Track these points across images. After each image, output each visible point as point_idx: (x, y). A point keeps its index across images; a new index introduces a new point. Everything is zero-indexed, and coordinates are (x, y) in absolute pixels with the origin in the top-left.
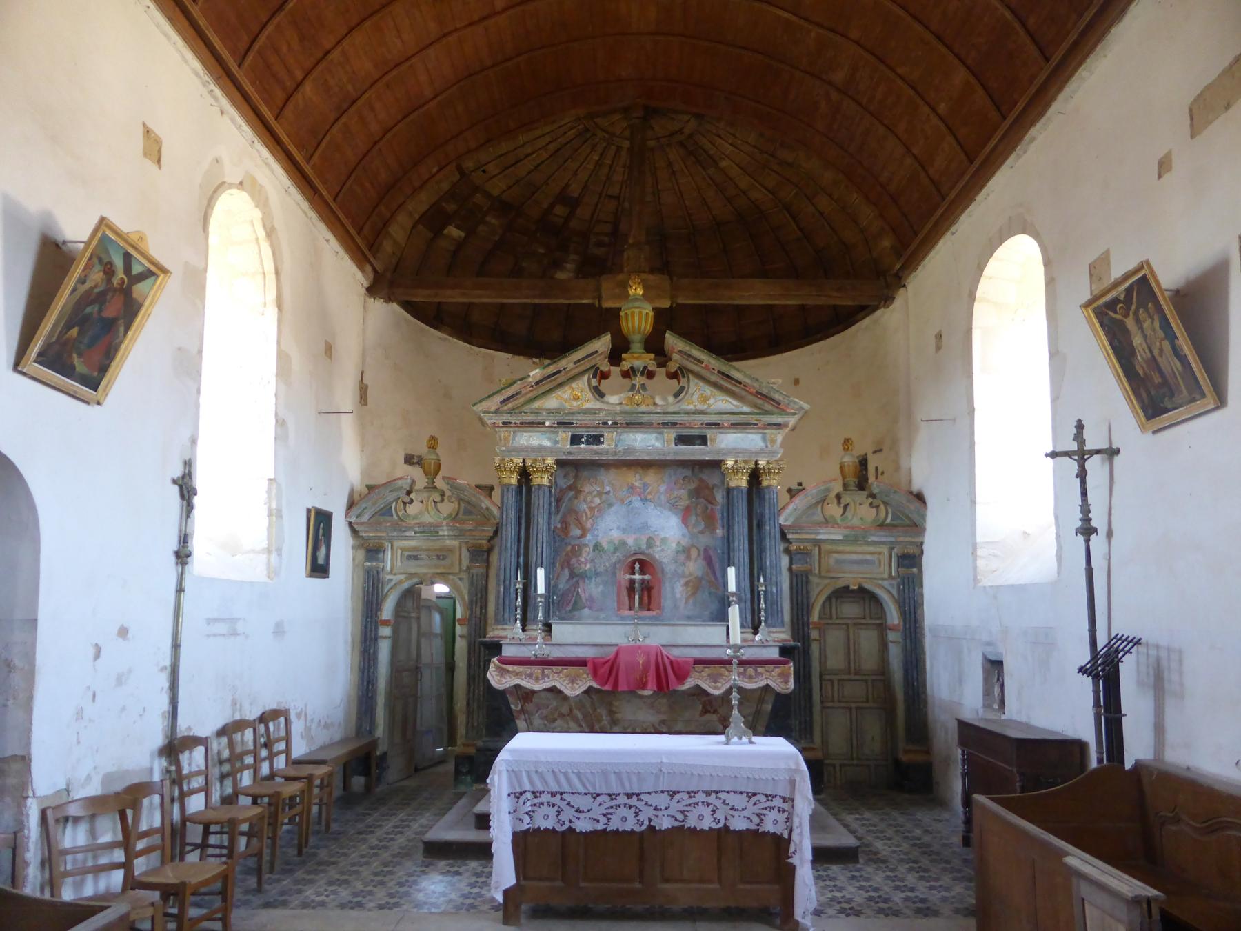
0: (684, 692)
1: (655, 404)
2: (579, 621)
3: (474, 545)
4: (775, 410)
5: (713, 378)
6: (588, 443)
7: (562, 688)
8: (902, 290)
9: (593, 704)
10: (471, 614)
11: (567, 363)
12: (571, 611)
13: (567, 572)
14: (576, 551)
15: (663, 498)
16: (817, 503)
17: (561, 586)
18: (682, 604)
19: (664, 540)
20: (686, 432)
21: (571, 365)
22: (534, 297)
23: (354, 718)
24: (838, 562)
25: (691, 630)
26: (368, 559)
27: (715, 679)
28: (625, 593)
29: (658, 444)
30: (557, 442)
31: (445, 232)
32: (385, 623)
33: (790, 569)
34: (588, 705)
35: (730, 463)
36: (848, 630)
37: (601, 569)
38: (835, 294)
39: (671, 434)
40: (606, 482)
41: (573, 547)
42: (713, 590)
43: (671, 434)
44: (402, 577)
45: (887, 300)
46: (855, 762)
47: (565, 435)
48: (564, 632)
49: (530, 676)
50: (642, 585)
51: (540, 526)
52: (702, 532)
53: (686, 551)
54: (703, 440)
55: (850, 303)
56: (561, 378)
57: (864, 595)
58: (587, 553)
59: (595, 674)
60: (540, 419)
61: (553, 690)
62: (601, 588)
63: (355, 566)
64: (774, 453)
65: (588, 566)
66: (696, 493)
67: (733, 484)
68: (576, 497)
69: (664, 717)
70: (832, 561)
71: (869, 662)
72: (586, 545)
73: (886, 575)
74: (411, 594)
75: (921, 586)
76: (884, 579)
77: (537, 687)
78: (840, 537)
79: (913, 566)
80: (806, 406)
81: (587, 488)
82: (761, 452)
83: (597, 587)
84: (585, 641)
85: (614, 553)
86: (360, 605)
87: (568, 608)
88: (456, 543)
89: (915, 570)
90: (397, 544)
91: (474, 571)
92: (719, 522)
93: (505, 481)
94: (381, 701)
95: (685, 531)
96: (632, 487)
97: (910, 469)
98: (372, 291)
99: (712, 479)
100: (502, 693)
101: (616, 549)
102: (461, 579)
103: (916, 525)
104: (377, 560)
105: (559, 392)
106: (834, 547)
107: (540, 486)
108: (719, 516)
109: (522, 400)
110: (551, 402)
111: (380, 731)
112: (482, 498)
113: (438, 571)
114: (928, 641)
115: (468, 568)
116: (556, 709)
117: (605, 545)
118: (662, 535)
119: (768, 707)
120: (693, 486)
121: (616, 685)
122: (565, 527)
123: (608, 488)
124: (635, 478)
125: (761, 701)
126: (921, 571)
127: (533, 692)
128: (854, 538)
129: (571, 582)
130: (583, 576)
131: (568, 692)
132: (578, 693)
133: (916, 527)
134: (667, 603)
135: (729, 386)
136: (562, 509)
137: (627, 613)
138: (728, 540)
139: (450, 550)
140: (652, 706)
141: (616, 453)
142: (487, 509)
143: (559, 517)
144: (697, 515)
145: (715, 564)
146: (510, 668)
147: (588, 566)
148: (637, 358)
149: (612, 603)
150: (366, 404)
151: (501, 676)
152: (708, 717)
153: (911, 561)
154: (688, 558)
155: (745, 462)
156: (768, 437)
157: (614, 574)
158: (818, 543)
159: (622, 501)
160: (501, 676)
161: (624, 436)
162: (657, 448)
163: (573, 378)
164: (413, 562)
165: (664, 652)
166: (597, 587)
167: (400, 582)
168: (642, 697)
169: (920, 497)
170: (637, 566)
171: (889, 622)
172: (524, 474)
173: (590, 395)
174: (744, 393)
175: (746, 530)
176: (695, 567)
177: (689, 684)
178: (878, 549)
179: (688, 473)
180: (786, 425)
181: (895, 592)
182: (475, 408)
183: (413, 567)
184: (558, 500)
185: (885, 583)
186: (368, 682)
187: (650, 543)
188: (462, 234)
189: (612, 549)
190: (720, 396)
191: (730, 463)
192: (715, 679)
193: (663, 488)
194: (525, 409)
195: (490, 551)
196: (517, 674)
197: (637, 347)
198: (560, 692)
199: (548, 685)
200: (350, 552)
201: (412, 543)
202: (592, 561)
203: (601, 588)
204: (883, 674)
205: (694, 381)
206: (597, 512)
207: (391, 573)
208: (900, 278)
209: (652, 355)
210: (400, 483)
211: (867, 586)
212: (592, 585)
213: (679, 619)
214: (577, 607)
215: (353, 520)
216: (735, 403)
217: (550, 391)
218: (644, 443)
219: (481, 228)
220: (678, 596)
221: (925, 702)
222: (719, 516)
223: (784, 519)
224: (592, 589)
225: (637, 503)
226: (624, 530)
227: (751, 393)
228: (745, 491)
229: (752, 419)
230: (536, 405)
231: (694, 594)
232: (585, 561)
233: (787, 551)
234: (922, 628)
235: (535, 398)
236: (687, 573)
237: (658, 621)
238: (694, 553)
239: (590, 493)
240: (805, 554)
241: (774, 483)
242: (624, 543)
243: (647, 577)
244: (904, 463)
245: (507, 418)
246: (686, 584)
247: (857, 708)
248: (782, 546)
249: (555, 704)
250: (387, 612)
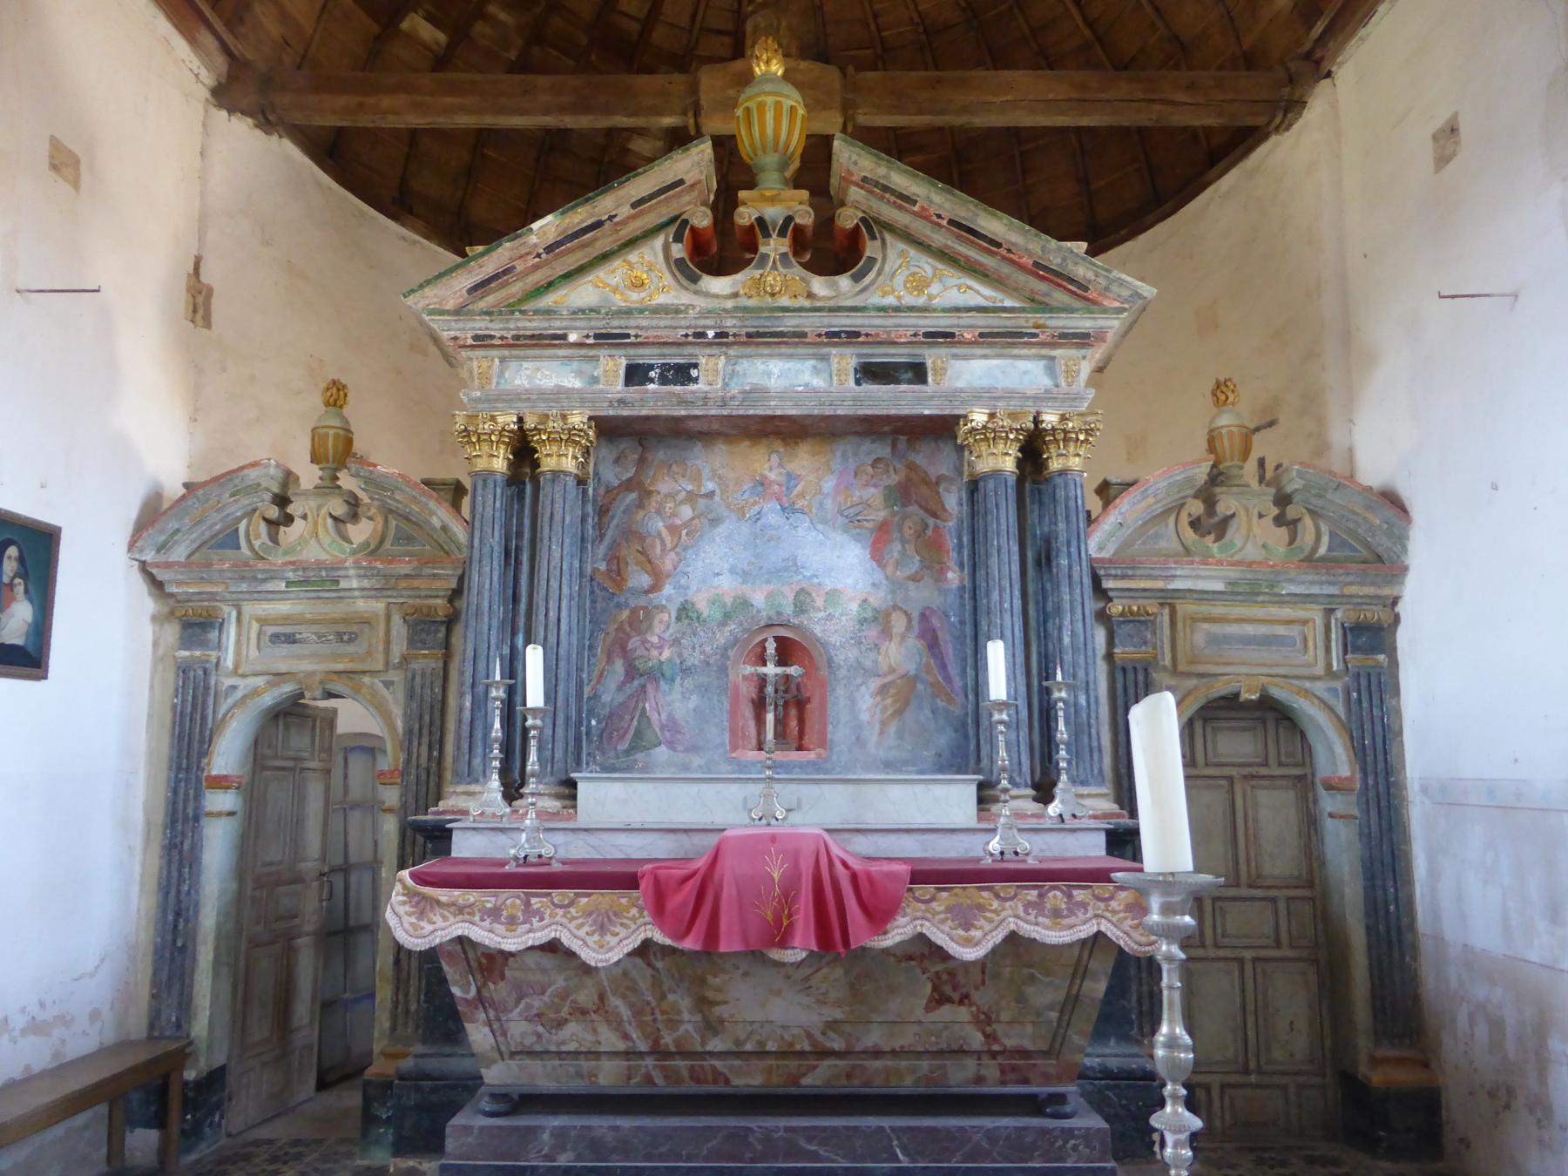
0: (886, 952)
1: (810, 295)
2: (646, 773)
3: (418, 610)
4: (1077, 304)
5: (940, 239)
6: (664, 380)
7: (575, 946)
8: (1324, 84)
9: (656, 983)
10: (408, 762)
11: (614, 202)
12: (627, 752)
13: (619, 666)
14: (640, 621)
15: (829, 504)
16: (1166, 513)
17: (606, 698)
18: (872, 736)
19: (833, 596)
20: (881, 355)
21: (625, 211)
22: (562, 109)
23: (145, 992)
24: (1214, 640)
25: (895, 791)
26: (186, 643)
27: (964, 918)
28: (748, 712)
29: (818, 382)
30: (595, 380)
31: (405, 25)
32: (221, 783)
33: (1109, 656)
34: (644, 985)
35: (979, 417)
36: (1232, 785)
37: (694, 659)
38: (1181, 97)
39: (846, 360)
40: (706, 473)
41: (634, 611)
42: (940, 703)
43: (846, 360)
44: (260, 681)
45: (1289, 107)
46: (1253, 1078)
47: (613, 364)
48: (602, 797)
49: (495, 913)
50: (786, 699)
51: (556, 561)
52: (915, 578)
53: (881, 619)
54: (918, 373)
55: (1211, 121)
56: (604, 241)
57: (1271, 714)
58: (663, 626)
59: (659, 908)
60: (556, 326)
61: (553, 947)
62: (694, 701)
63: (158, 660)
64: (1076, 398)
65: (666, 654)
66: (902, 494)
67: (984, 465)
68: (640, 505)
69: (838, 1014)
70: (1199, 639)
71: (1279, 860)
72: (662, 608)
73: (1319, 670)
74: (289, 713)
75: (1396, 691)
76: (1318, 678)
77: (511, 944)
78: (1219, 586)
79: (1374, 649)
80: (1148, 291)
81: (664, 486)
82: (1047, 397)
83: (685, 697)
84: (636, 820)
85: (723, 624)
86: (165, 745)
87: (623, 746)
88: (379, 606)
89: (1381, 657)
90: (250, 609)
91: (416, 666)
92: (954, 555)
93: (481, 464)
94: (205, 955)
95: (878, 576)
96: (763, 483)
97: (1351, 450)
98: (224, 95)
99: (935, 461)
100: (431, 956)
101: (727, 616)
102: (388, 684)
103: (1380, 559)
104: (204, 644)
105: (601, 273)
106: (1204, 609)
107: (557, 474)
108: (951, 542)
109: (517, 288)
110: (583, 293)
111: (200, 1027)
112: (432, 505)
113: (340, 667)
114: (1418, 814)
115: (405, 659)
116: (564, 995)
117: (703, 606)
118: (829, 584)
119: (1098, 987)
120: (894, 479)
121: (712, 935)
122: (617, 570)
123: (710, 486)
124: (767, 463)
125: (1080, 971)
126: (1394, 663)
127: (506, 955)
128: (1246, 592)
129: (629, 689)
130: (655, 675)
131: (588, 956)
132: (615, 956)
133: (1385, 564)
134: (839, 733)
135: (973, 254)
136: (610, 534)
137: (753, 755)
138: (974, 593)
139: (366, 622)
140: (806, 986)
141: (724, 403)
142: (445, 528)
143: (602, 549)
144: (903, 541)
145: (951, 647)
146: (443, 894)
147: (666, 654)
148: (772, 200)
149: (718, 735)
150: (208, 324)
151: (421, 915)
152: (945, 1012)
153: (1372, 636)
154: (886, 633)
155: (1013, 416)
156: (1060, 367)
157: (723, 670)
158: (1168, 599)
159: (741, 512)
160: (421, 915)
161: (744, 365)
162: (815, 391)
163: (631, 243)
164: (284, 649)
165: (836, 850)
166: (685, 697)
167: (256, 692)
168: (779, 965)
169: (1392, 501)
170: (771, 647)
171: (1323, 769)
172: (523, 450)
173: (668, 279)
174: (1006, 269)
175: (1016, 568)
176: (902, 654)
177: (899, 932)
178: (1300, 613)
179: (883, 450)
180: (1100, 336)
181: (1341, 710)
182: (410, 301)
183: (282, 659)
184: (603, 512)
185: (1319, 687)
186: (178, 914)
187: (802, 602)
188: (442, 37)
189: (718, 615)
190: (953, 278)
191: (979, 417)
192: (964, 918)
193: (828, 485)
194: (529, 306)
195: (451, 621)
196: (460, 910)
197: (771, 181)
198: (571, 955)
199: (540, 937)
200: (147, 631)
201: (284, 608)
202: (676, 642)
203: (694, 701)
204: (1310, 885)
205: (895, 246)
206: (686, 536)
207: (235, 672)
208: (1318, 63)
209: (805, 194)
210: (253, 474)
211: (1276, 693)
212: (676, 695)
213: (867, 768)
214: (640, 743)
215: (149, 556)
216: (987, 291)
217: (581, 270)
218: (789, 380)
219: (480, 28)
220: (865, 717)
221: (1415, 948)
222: (951, 542)
223: (1100, 542)
224: (675, 703)
225: (772, 514)
226: (745, 576)
227: (1022, 268)
228: (1012, 480)
229: (1025, 321)
230: (548, 300)
231: (899, 713)
232: (661, 641)
233: (1102, 617)
234: (1400, 786)
235: (550, 286)
236: (884, 667)
237: (820, 773)
238: (898, 623)
239: (671, 496)
240: (1140, 621)
241: (1075, 463)
242: (744, 604)
243: (794, 670)
244: (1336, 436)
245: (481, 325)
246: (883, 690)
247: (1255, 960)
248: (1092, 605)
249: (561, 982)
250: (228, 753)
